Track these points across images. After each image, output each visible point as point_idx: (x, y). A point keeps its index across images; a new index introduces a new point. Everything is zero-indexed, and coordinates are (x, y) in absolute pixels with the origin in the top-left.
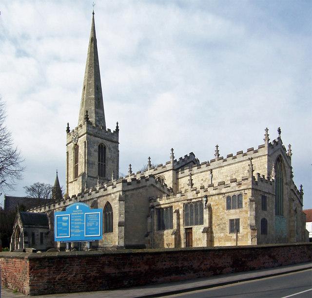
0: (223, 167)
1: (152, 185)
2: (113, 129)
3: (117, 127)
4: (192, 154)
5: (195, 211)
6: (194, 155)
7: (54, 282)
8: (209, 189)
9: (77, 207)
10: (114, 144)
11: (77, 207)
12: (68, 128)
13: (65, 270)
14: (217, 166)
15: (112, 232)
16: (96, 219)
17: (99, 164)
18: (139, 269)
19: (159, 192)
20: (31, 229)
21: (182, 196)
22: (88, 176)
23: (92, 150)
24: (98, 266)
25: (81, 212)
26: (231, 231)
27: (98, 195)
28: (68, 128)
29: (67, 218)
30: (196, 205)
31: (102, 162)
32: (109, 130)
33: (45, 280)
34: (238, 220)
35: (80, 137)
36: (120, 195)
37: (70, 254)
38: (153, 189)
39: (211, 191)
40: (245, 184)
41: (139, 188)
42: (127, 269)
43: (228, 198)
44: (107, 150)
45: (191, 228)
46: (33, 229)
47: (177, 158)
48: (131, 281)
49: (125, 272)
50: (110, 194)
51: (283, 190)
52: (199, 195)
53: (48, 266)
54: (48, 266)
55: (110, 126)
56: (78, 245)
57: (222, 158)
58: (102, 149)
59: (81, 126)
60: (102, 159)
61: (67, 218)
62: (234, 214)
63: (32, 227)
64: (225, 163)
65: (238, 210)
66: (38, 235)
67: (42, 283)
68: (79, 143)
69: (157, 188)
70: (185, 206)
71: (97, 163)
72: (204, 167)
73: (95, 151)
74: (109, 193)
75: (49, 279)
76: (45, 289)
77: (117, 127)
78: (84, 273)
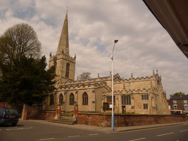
0: (135, 82)
2: (73, 57)
3: (75, 56)
5: (126, 99)
8: (133, 91)
10: (73, 64)
12: (51, 54)
14: (132, 81)
15: (87, 104)
22: (61, 77)
26: (144, 108)
27: (79, 88)
28: (51, 54)
30: (127, 97)
32: (72, 57)
34: (147, 104)
36: (93, 90)
38: (104, 88)
39: (134, 92)
40: (149, 91)
43: (142, 95)
44: (70, 66)
51: (66, 75)
52: (129, 93)
55: (72, 55)
56: (129, 113)
57: (134, 79)
58: (68, 65)
62: (145, 102)
64: (136, 81)
65: (147, 101)
70: (122, 97)
72: (122, 81)
73: (65, 66)
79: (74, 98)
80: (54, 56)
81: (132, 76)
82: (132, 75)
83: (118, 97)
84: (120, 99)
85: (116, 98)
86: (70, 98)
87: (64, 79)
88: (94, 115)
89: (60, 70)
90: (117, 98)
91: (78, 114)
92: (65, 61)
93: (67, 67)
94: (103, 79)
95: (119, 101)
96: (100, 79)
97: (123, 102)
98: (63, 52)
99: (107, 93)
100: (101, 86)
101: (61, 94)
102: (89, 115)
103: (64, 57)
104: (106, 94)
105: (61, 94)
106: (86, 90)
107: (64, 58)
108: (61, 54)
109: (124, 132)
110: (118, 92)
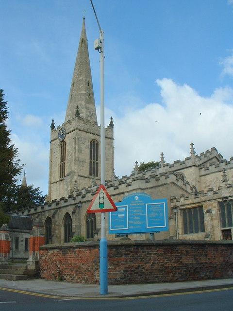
1: (173, 183)
3: (112, 122)
4: (214, 149)
6: (217, 151)
7: (131, 271)
9: (137, 198)
11: (137, 198)
12: (53, 124)
13: (142, 259)
16: (160, 210)
17: (91, 162)
18: (215, 261)
19: (180, 191)
20: (16, 233)
21: (214, 194)
23: (83, 147)
24: (176, 255)
25: (142, 203)
28: (53, 124)
29: (124, 209)
31: (94, 159)
33: (122, 267)
35: (68, 133)
37: (147, 242)
38: (175, 187)
41: (159, 186)
42: (203, 260)
45: (230, 230)
46: (18, 233)
47: (198, 153)
48: (208, 274)
49: (202, 263)
50: (123, 193)
51: (90, 167)
53: (125, 254)
54: (125, 254)
57: (168, 165)
59: (69, 122)
60: (94, 156)
61: (124, 209)
63: (17, 232)
66: (22, 241)
67: (119, 273)
68: (66, 140)
69: (178, 186)
70: (221, 205)
71: (88, 160)
74: (121, 191)
75: (125, 268)
76: (121, 278)
77: (112, 122)
78: (162, 263)
79: (95, 220)
80: (59, 127)
81: (193, 152)
82: (193, 149)
83: (210, 208)
84: (215, 211)
85: (205, 211)
86: (87, 222)
87: (86, 179)
88: (77, 247)
89: (73, 159)
90: (208, 211)
91: (40, 249)
92: (84, 134)
93: (91, 151)
94: (175, 165)
95: (214, 217)
96: (168, 167)
97: (228, 220)
98: (77, 114)
99: (182, 199)
100: (163, 180)
101: (67, 214)
102: (67, 249)
103: (81, 125)
104: (179, 204)
105: (67, 214)
106: (122, 195)
107: (82, 128)
108: (74, 119)
109: (218, 290)
110: (210, 193)
